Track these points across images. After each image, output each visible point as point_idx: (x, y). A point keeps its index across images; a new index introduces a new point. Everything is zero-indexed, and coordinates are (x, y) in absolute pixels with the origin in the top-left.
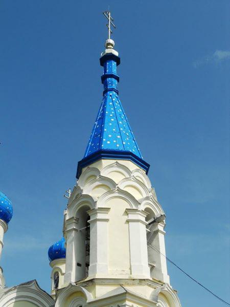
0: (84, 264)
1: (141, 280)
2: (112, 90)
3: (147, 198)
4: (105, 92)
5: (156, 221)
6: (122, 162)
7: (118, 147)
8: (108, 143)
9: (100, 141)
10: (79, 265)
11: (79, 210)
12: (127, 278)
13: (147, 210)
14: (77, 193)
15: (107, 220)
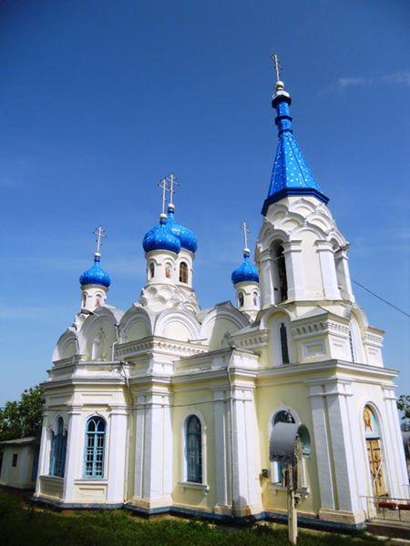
0: (283, 290)
1: (334, 301)
2: (287, 130)
3: (333, 230)
4: (281, 132)
5: (342, 249)
6: (306, 198)
7: (302, 184)
8: (293, 180)
9: (284, 180)
10: (275, 289)
11: (273, 242)
12: (322, 299)
13: (333, 240)
14: (267, 230)
15: (300, 251)
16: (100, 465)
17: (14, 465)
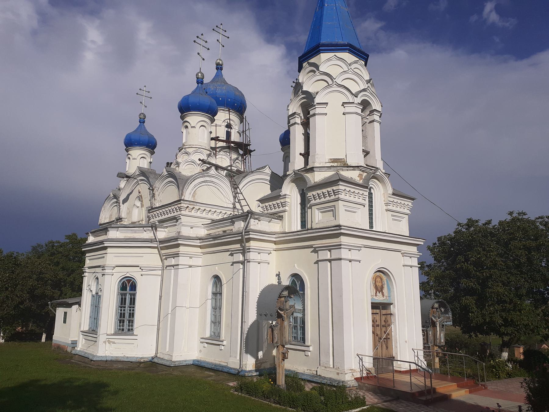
6: (340, 55)
16: (131, 322)
17: (65, 322)
